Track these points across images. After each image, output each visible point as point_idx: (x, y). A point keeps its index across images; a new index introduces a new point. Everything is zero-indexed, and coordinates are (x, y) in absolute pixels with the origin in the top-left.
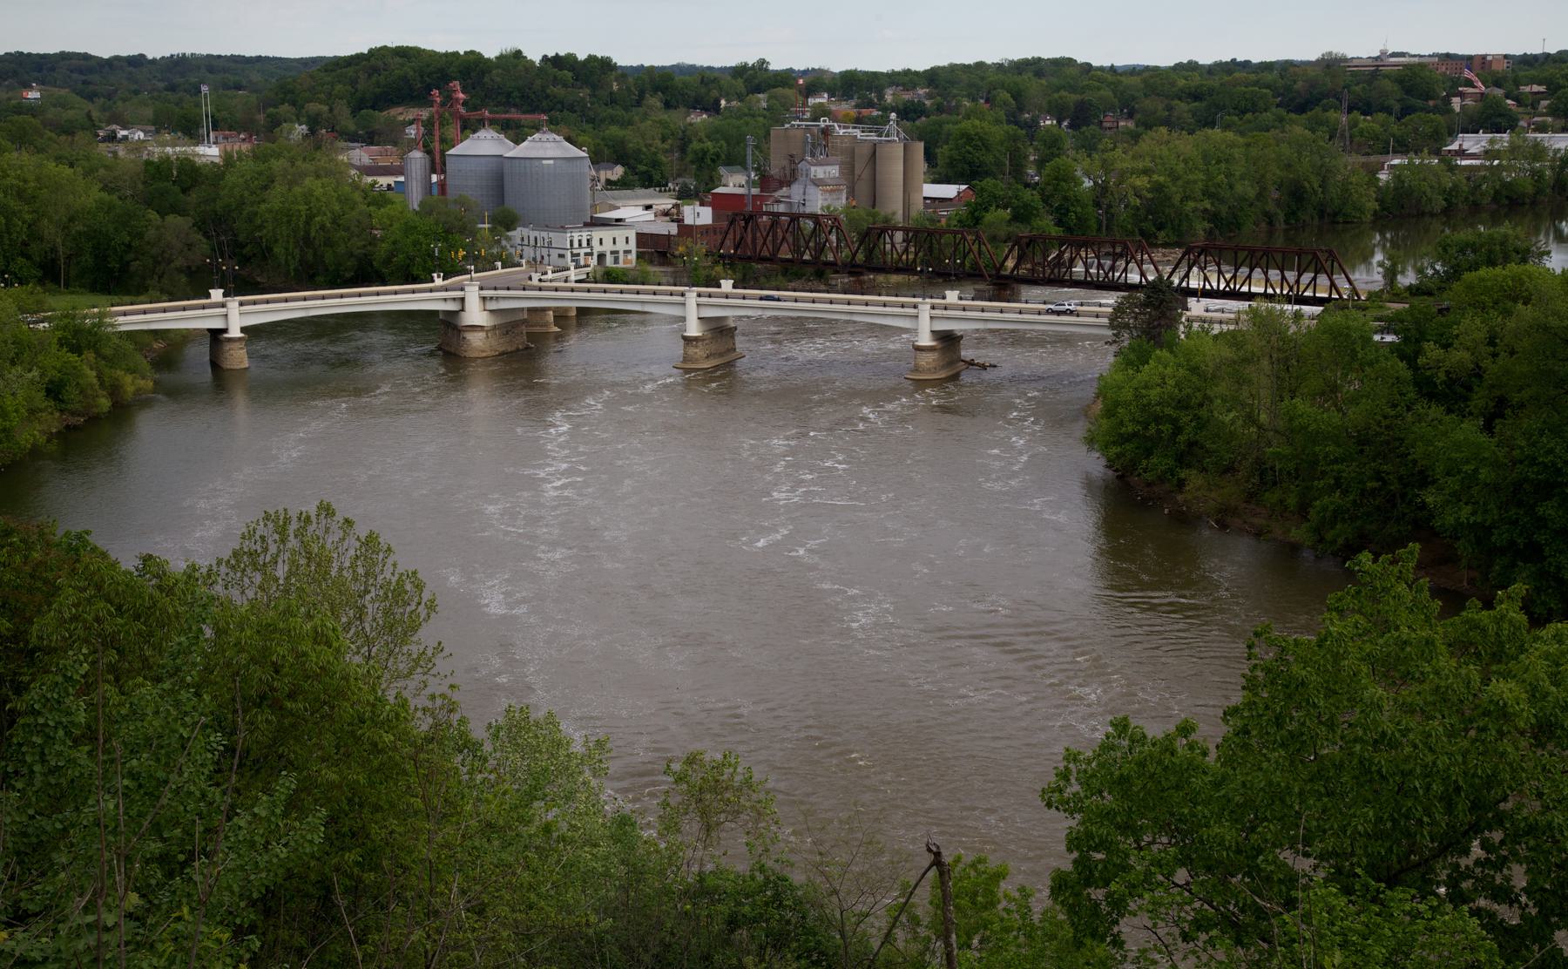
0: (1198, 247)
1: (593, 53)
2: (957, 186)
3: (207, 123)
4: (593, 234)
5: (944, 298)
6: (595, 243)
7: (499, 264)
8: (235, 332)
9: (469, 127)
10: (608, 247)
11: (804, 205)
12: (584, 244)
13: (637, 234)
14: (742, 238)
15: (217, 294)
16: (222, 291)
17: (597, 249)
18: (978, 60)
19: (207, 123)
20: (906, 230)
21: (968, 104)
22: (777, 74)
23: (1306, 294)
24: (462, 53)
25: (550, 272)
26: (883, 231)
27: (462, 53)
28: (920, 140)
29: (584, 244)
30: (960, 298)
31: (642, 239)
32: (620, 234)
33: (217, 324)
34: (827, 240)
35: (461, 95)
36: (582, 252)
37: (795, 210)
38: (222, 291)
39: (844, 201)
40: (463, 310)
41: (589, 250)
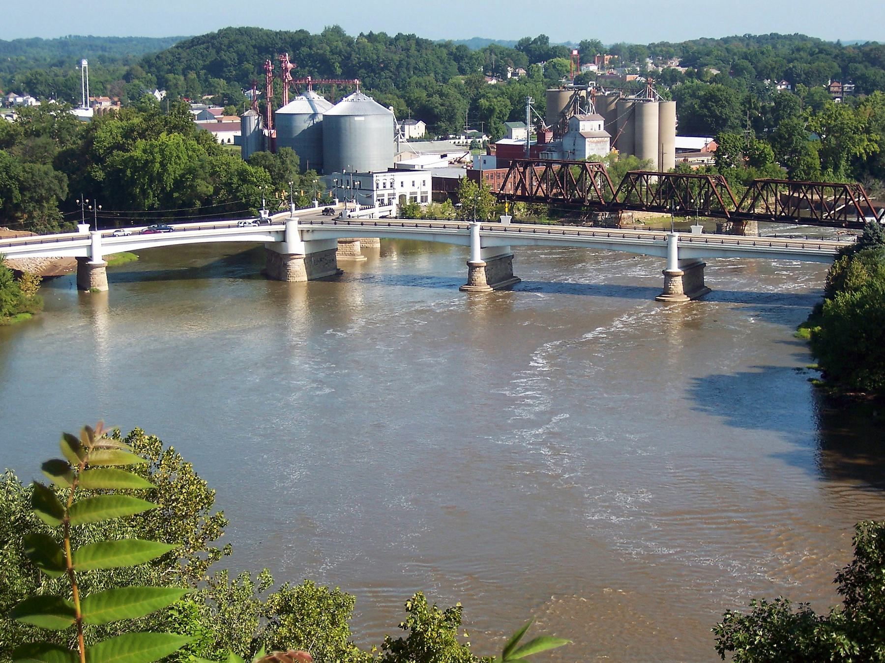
0: (761, 181)
1: (91, 34)
2: (705, 139)
3: (86, 90)
4: (395, 178)
5: (499, 221)
6: (397, 185)
7: (316, 203)
8: (97, 260)
9: (297, 91)
10: (407, 190)
11: (574, 153)
12: (388, 186)
13: (433, 178)
14: (521, 180)
15: (84, 228)
16: (89, 225)
17: (399, 191)
18: (476, 36)
19: (86, 90)
20: (660, 175)
21: (32, 63)
22: (555, 49)
23: (840, 219)
24: (793, 34)
25: (357, 209)
26: (641, 175)
27: (793, 34)
28: (673, 100)
29: (388, 186)
30: (703, 232)
31: (437, 183)
32: (417, 177)
33: (83, 253)
34: (592, 183)
35: (290, 65)
36: (386, 193)
37: (567, 159)
38: (89, 225)
39: (608, 151)
40: (284, 241)
41: (392, 191)
